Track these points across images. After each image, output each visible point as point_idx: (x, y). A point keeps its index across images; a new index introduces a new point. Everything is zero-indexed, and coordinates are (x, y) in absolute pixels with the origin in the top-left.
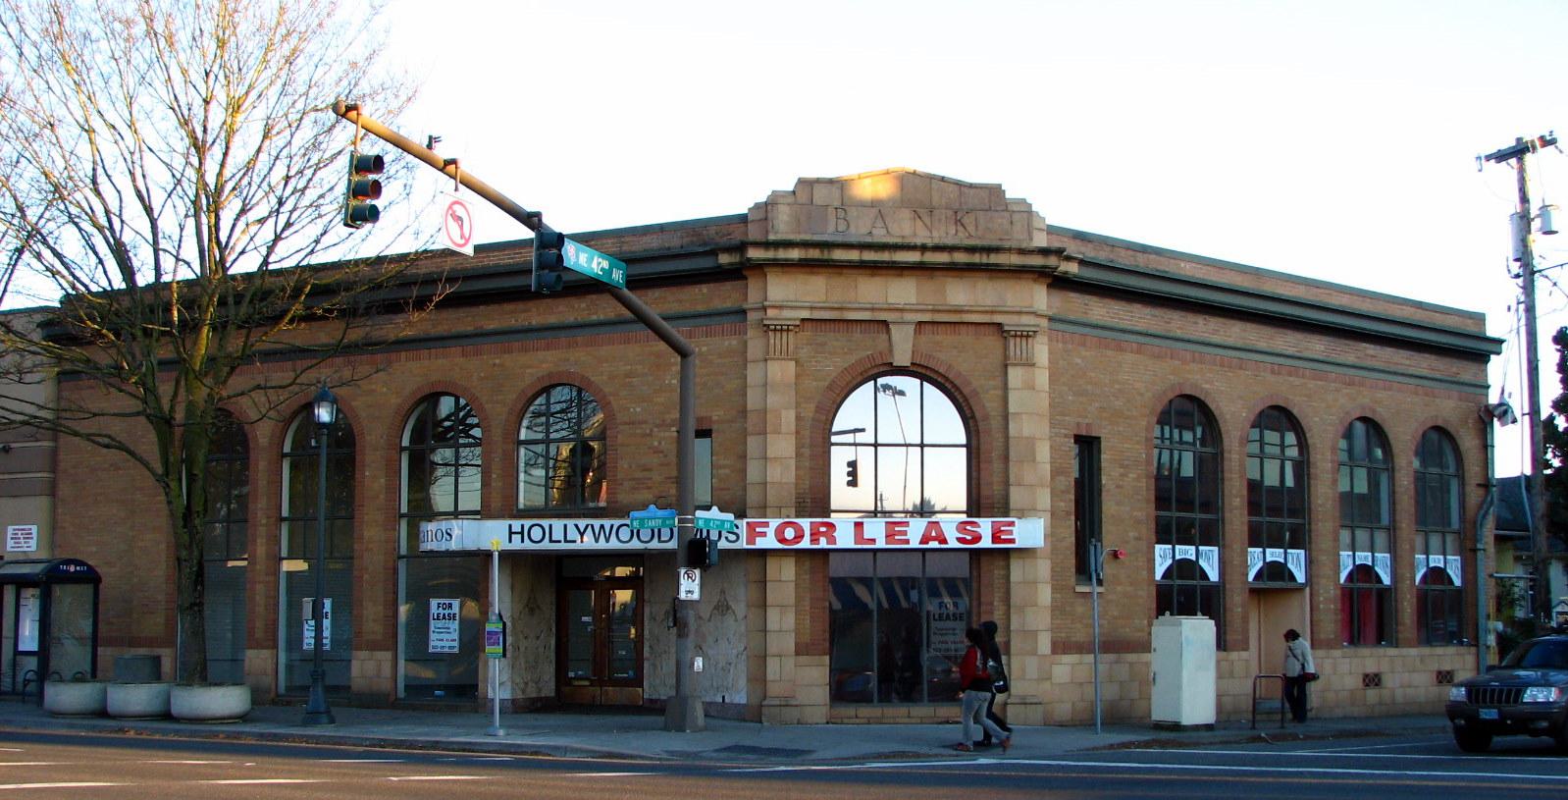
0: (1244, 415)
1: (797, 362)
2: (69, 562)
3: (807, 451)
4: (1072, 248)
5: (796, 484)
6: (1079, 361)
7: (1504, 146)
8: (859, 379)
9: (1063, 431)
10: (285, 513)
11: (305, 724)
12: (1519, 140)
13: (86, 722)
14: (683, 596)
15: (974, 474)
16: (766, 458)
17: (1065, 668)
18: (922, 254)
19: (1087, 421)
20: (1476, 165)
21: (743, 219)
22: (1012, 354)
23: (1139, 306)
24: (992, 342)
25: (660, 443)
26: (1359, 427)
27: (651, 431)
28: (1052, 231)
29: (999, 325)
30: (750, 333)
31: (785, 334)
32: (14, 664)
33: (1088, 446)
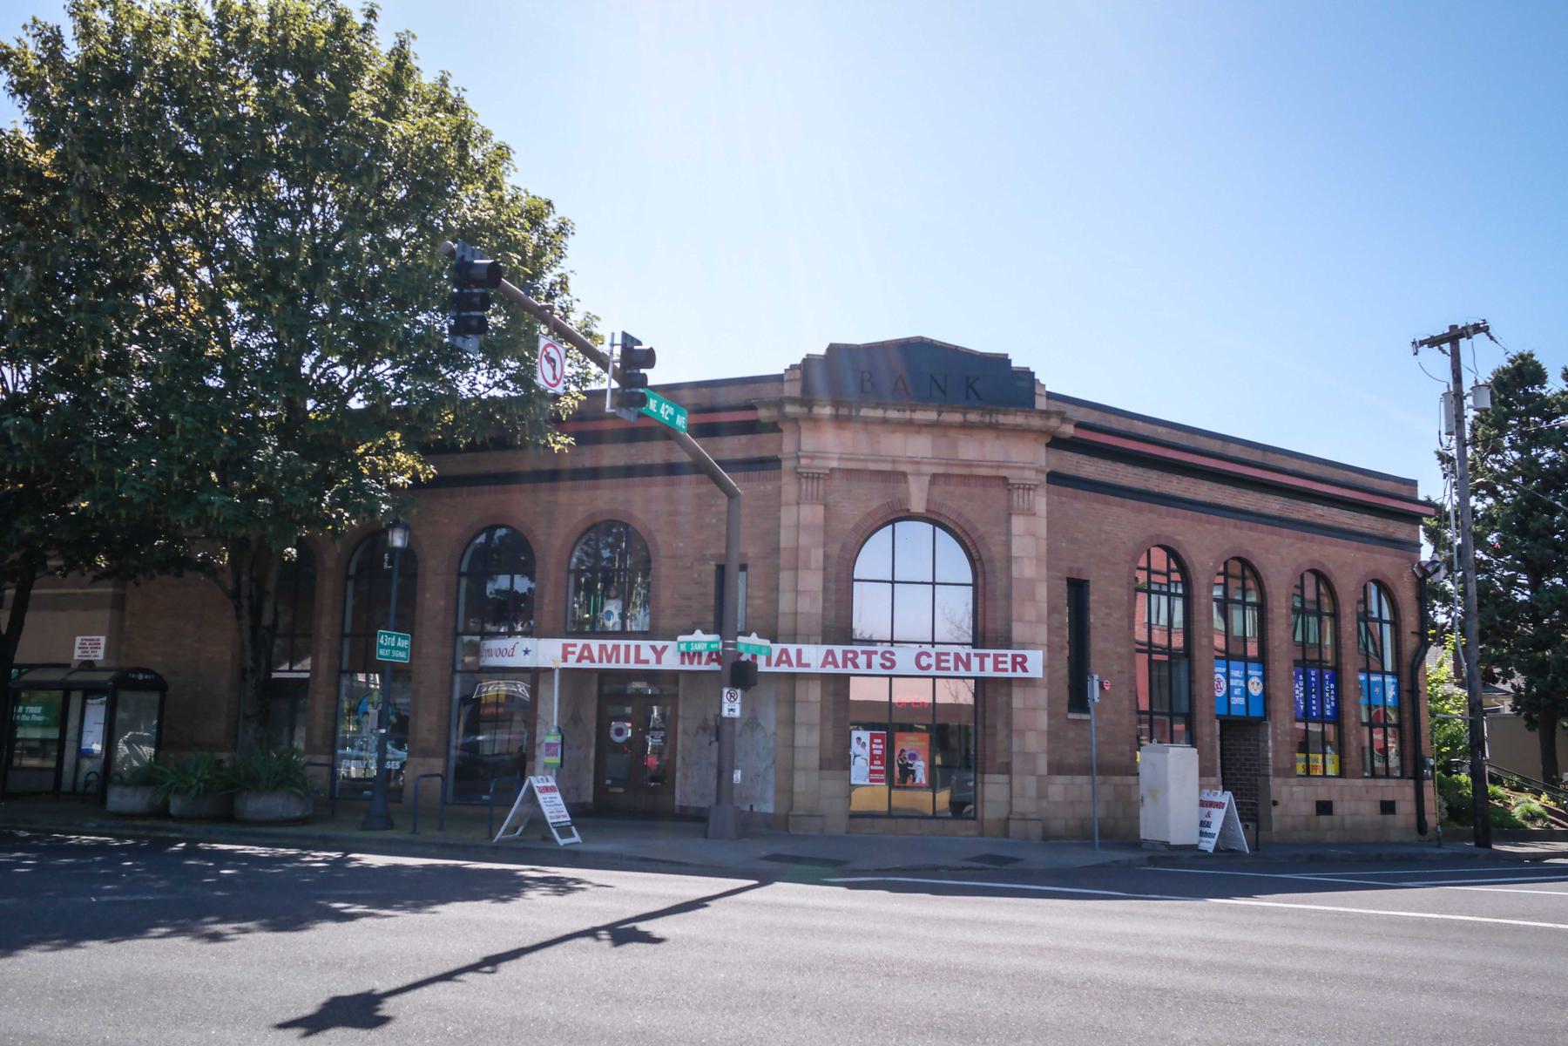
1: (826, 506)
2: (138, 670)
3: (833, 586)
4: (1070, 411)
5: (823, 615)
7: (1437, 333)
8: (881, 523)
10: (348, 630)
11: (364, 828)
13: (146, 823)
14: (725, 713)
15: (980, 610)
16: (797, 591)
17: (1059, 787)
20: (1411, 350)
21: (778, 379)
22: (1015, 504)
23: (1122, 465)
24: (997, 493)
25: (700, 575)
26: (1310, 581)
27: (692, 564)
28: (1051, 396)
29: (1005, 478)
30: (785, 479)
31: (810, 481)
32: (78, 766)
33: (1078, 590)
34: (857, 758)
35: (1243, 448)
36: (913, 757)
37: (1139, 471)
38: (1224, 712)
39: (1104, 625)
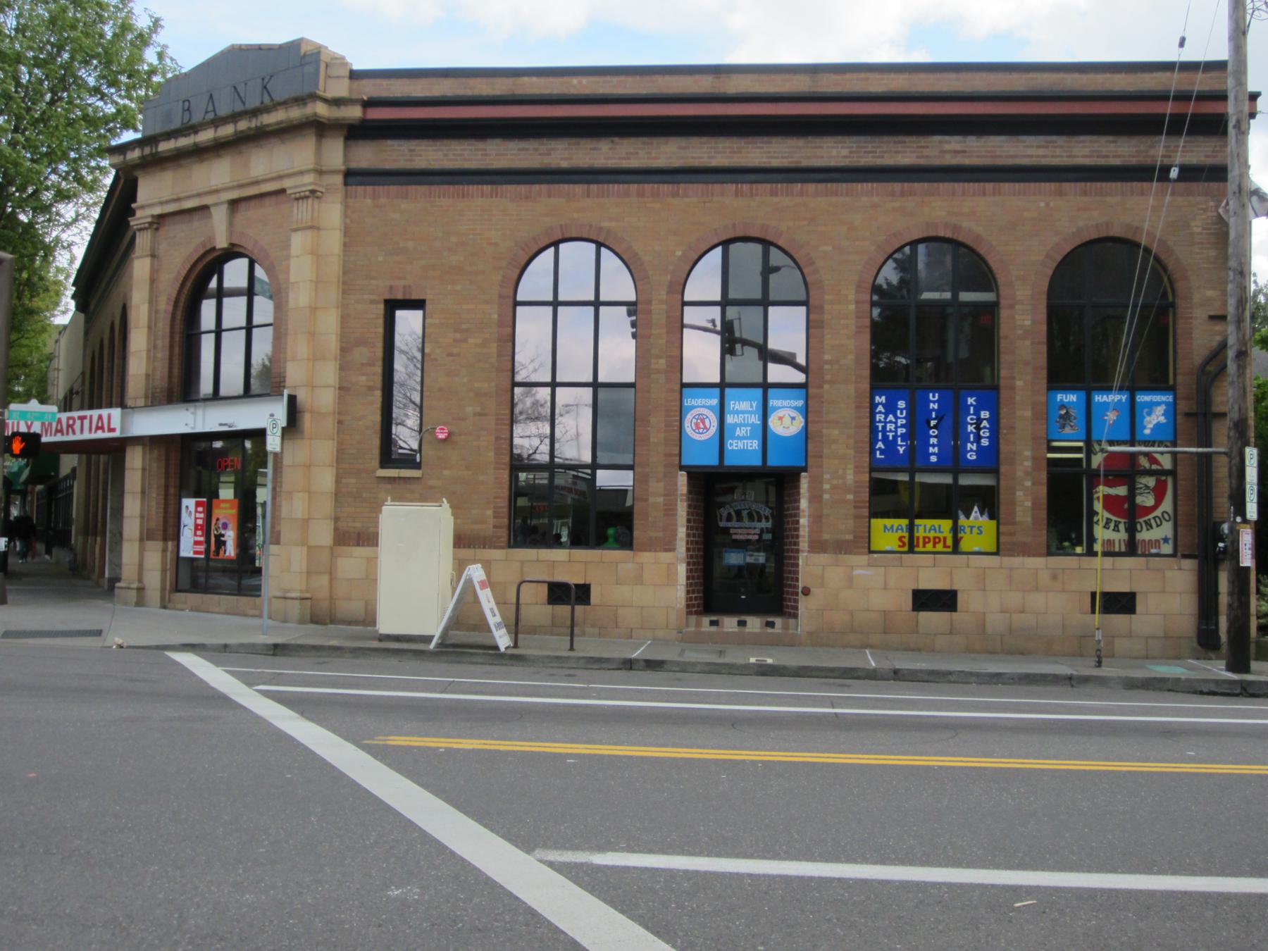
0: (679, 253)
5: (147, 376)
6: (397, 216)
9: (366, 297)
12: (162, 27)
18: (216, 131)
19: (403, 283)
34: (186, 528)
35: (756, 76)
36: (225, 526)
37: (531, 145)
38: (711, 460)
39: (450, 355)
